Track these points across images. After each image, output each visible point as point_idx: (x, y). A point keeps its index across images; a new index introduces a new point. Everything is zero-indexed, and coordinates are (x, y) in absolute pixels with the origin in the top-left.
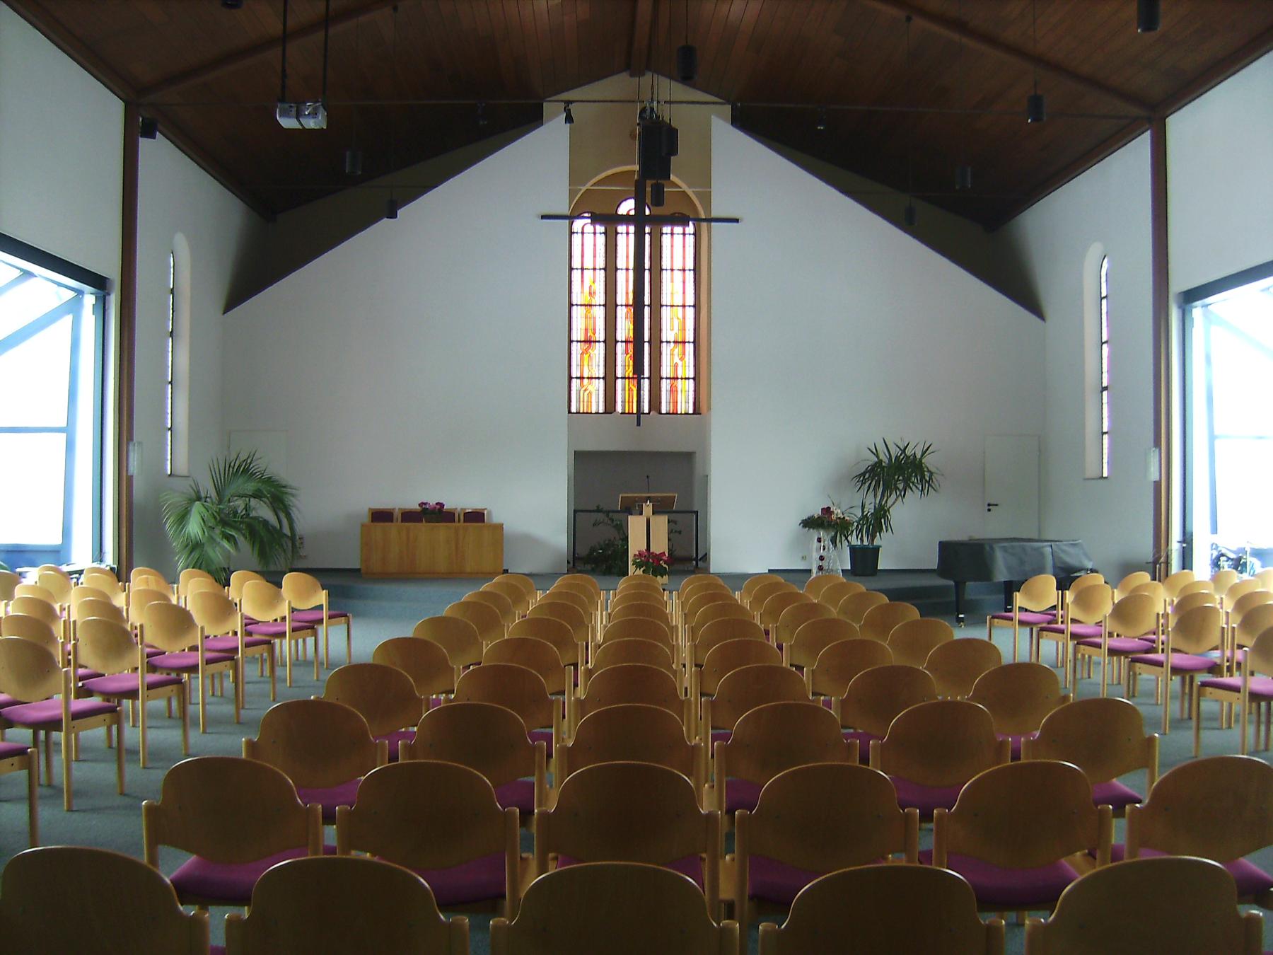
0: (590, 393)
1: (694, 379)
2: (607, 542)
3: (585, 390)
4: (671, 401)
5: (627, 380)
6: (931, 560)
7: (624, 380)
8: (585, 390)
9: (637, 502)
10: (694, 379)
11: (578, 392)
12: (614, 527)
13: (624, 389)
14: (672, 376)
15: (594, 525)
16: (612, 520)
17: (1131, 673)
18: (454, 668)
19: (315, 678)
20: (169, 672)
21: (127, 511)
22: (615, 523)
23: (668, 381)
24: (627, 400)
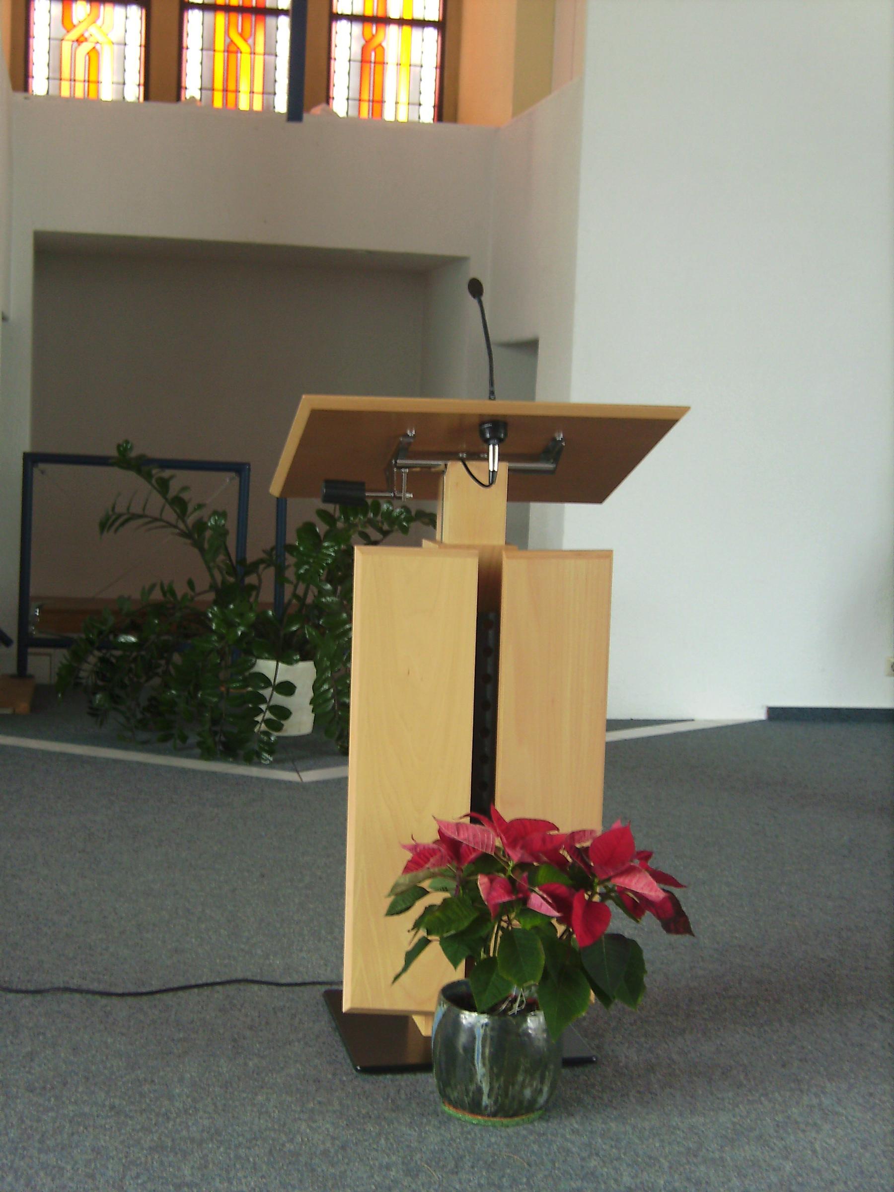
0: (94, 55)
1: (440, 26)
2: (157, 595)
3: (79, 41)
4: (365, 96)
5: (221, 18)
6: (762, 715)
7: (209, 16)
8: (79, 41)
9: (404, 450)
10: (440, 26)
11: (56, 43)
12: (187, 535)
13: (208, 47)
14: (369, 13)
15: (104, 526)
16: (179, 504)
17: (789, 1150)
18: (862, 1149)
19: (300, 1140)
20: (348, 1123)
21: (425, 464)
22: (191, 520)
23: (357, 28)
24: (219, 84)
